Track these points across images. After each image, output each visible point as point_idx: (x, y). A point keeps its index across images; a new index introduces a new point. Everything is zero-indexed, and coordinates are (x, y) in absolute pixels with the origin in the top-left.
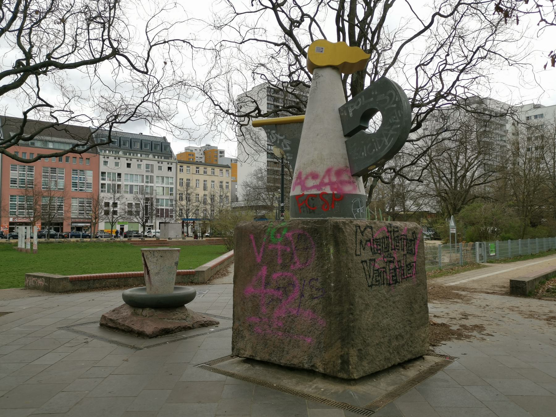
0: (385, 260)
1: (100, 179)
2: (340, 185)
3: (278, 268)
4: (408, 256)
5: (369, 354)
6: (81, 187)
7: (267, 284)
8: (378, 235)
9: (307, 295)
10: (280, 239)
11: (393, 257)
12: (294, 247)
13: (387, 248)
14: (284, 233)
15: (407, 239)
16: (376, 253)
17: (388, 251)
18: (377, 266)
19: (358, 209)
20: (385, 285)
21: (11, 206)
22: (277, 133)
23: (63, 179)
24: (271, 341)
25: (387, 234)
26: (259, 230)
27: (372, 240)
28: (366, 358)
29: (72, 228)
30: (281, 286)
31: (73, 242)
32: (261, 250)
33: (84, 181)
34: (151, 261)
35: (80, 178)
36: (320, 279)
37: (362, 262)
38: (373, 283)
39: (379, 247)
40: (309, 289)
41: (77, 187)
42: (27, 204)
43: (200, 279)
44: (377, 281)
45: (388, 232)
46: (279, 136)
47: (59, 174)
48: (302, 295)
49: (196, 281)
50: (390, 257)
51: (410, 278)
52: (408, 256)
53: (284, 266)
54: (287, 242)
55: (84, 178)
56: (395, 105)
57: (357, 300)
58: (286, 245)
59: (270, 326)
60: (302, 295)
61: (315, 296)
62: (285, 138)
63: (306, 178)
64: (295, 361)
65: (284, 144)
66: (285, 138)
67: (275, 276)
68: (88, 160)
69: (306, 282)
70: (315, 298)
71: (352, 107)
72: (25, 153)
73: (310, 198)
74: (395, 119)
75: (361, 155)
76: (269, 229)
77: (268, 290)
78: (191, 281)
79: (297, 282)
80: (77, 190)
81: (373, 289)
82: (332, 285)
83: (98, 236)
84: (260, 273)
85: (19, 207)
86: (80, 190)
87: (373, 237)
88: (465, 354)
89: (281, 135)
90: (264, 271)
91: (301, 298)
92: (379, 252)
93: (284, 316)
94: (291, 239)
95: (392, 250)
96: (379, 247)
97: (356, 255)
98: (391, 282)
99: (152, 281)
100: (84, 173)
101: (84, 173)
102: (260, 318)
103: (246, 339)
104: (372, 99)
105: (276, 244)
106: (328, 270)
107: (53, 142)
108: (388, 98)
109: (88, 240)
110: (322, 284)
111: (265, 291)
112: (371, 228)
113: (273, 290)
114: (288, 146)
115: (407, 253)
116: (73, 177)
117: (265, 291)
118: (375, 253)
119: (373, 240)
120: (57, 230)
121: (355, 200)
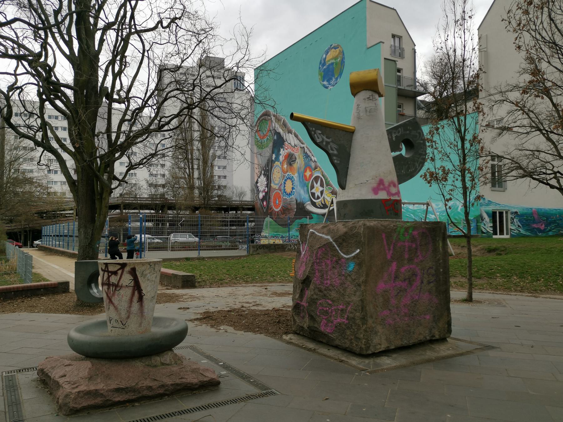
3: (406, 262)
7: (396, 277)
9: (425, 281)
10: (408, 237)
12: (419, 243)
14: (410, 231)
22: (322, 134)
24: (399, 327)
26: (389, 229)
30: (407, 277)
32: (391, 248)
34: (148, 279)
36: (434, 267)
40: (427, 276)
46: (325, 138)
48: (422, 282)
53: (410, 260)
54: (413, 240)
56: (422, 142)
58: (412, 242)
59: (398, 315)
60: (422, 282)
61: (431, 281)
62: (332, 141)
63: (389, 185)
64: (421, 338)
65: (331, 147)
66: (332, 141)
67: (403, 270)
69: (425, 271)
70: (431, 283)
71: (395, 133)
73: (395, 203)
74: (422, 151)
75: (401, 172)
76: (399, 229)
77: (397, 283)
79: (419, 272)
82: (441, 270)
84: (390, 269)
89: (327, 137)
90: (394, 265)
91: (421, 284)
93: (409, 302)
94: (417, 236)
99: (146, 310)
102: (390, 310)
103: (379, 334)
104: (408, 132)
105: (404, 242)
106: (439, 260)
108: (418, 134)
110: (435, 271)
111: (394, 284)
113: (400, 282)
114: (334, 149)
117: (394, 284)
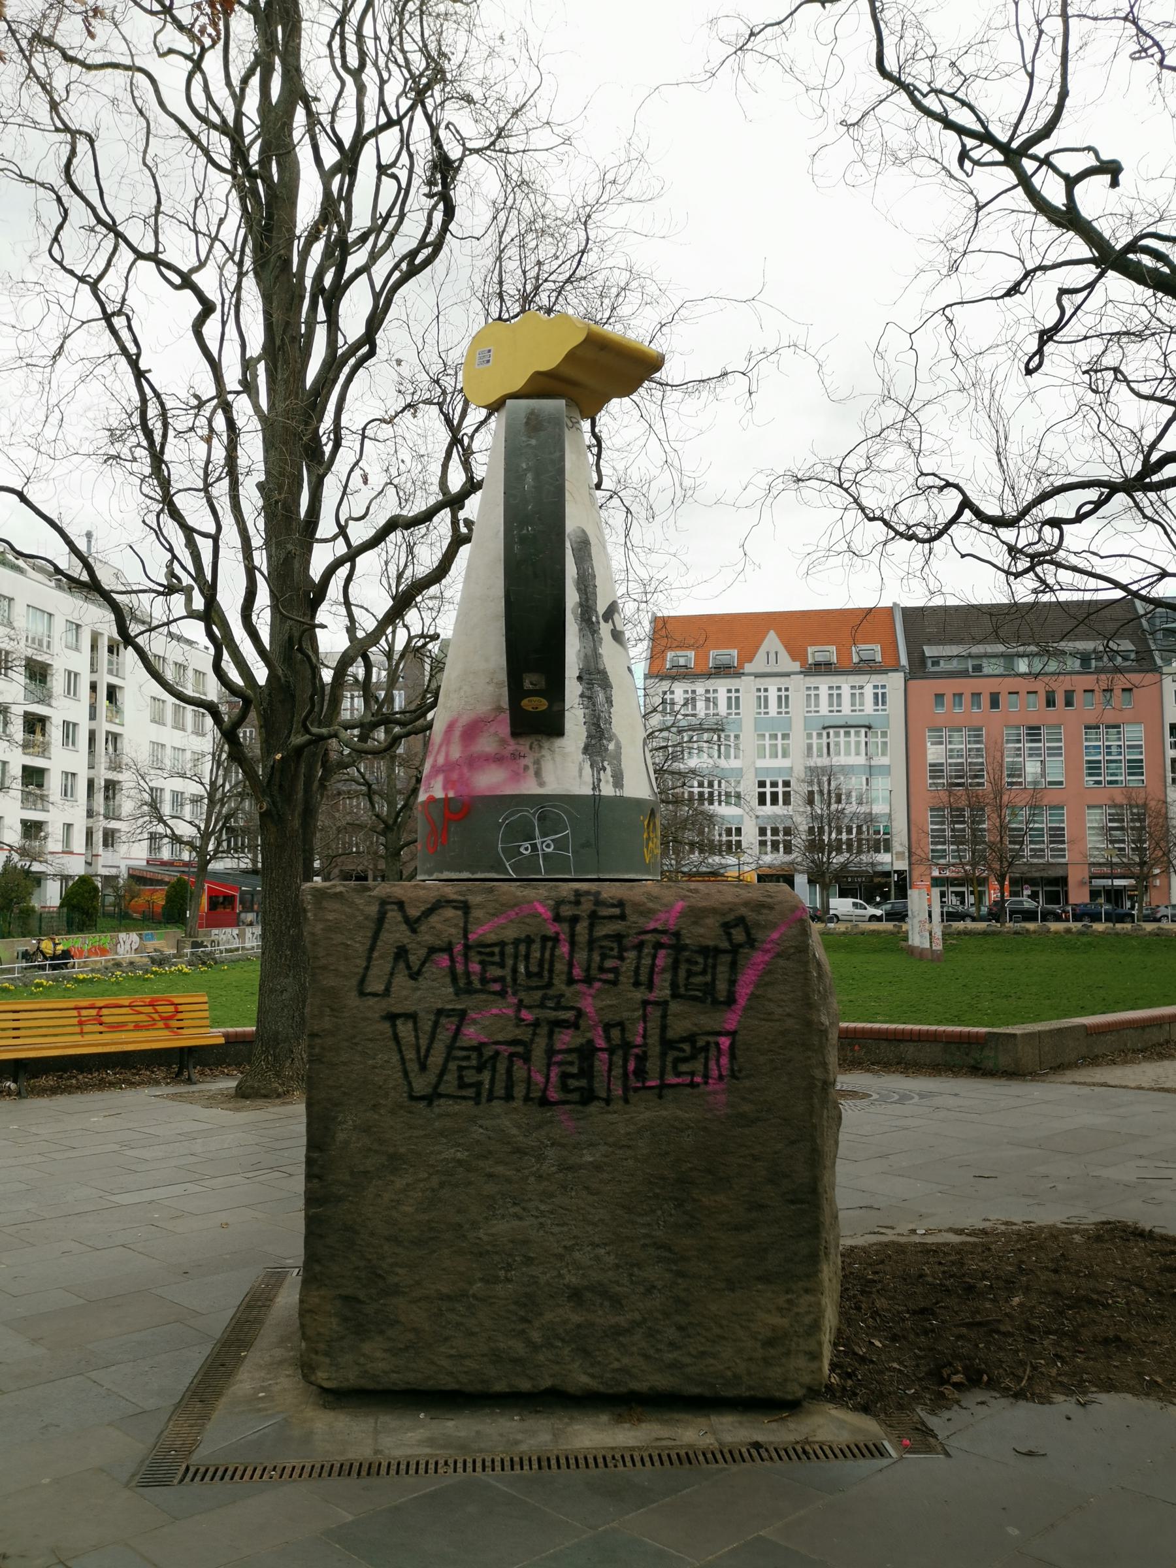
0: (525, 1014)
1: (1168, 745)
2: (465, 770)
4: (675, 1007)
5: (398, 1322)
6: (1112, 775)
8: (484, 931)
11: (572, 1008)
13: (539, 975)
15: (678, 948)
16: (476, 991)
17: (549, 985)
18: (472, 1033)
19: (527, 844)
20: (517, 1104)
21: (933, 837)
23: (1060, 755)
25: (551, 929)
27: (458, 949)
28: (382, 1332)
29: (1094, 894)
31: (1056, 933)
33: (1120, 754)
35: (1109, 747)
37: (392, 1018)
38: (442, 1089)
39: (495, 972)
41: (1099, 775)
42: (953, 830)
43: (1004, 1061)
44: (462, 1085)
45: (557, 918)
47: (1049, 740)
49: (989, 1064)
50: (554, 1009)
51: (689, 1090)
52: (675, 1007)
55: (1120, 746)
57: (341, 1136)
68: (1127, 694)
72: (961, 695)
78: (972, 1062)
80: (1099, 782)
81: (436, 1110)
83: (1159, 915)
85: (1051, 836)
86: (1110, 782)
87: (466, 937)
88: (1030, 1454)
92: (496, 987)
95: (571, 981)
96: (495, 972)
97: (362, 994)
98: (554, 1095)
100: (1119, 733)
101: (1119, 733)
107: (1028, 656)
109: (1128, 926)
112: (465, 907)
115: (675, 996)
116: (1087, 747)
118: (469, 990)
119: (467, 947)
120: (1053, 898)
121: (512, 814)
